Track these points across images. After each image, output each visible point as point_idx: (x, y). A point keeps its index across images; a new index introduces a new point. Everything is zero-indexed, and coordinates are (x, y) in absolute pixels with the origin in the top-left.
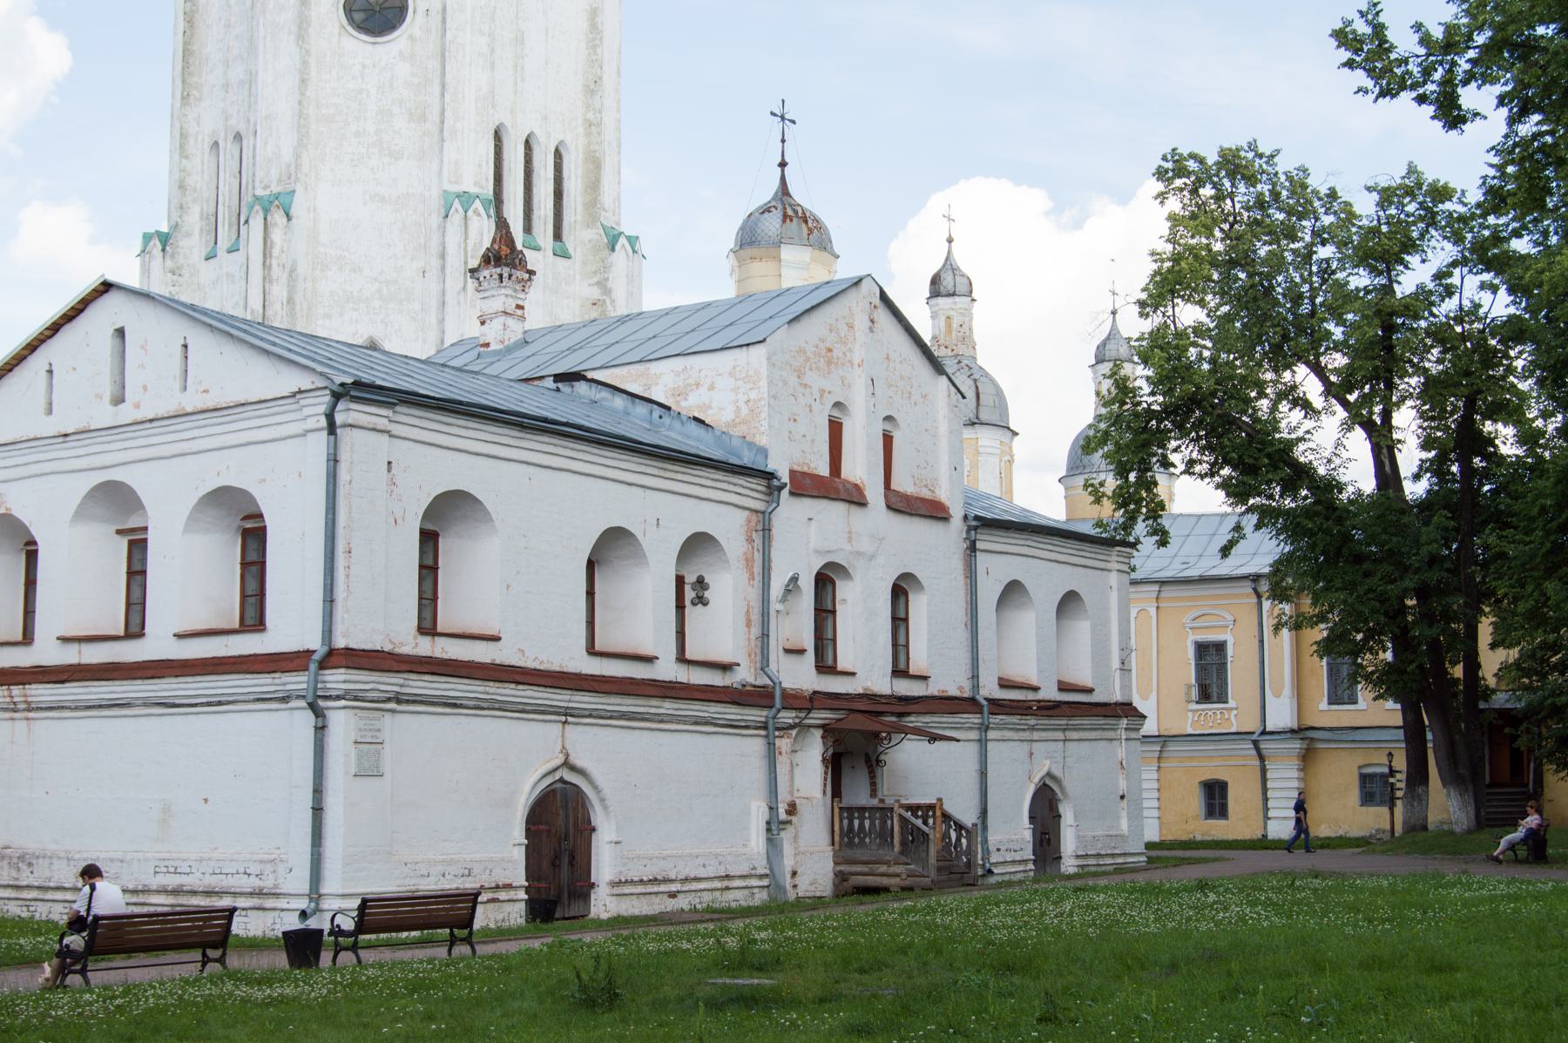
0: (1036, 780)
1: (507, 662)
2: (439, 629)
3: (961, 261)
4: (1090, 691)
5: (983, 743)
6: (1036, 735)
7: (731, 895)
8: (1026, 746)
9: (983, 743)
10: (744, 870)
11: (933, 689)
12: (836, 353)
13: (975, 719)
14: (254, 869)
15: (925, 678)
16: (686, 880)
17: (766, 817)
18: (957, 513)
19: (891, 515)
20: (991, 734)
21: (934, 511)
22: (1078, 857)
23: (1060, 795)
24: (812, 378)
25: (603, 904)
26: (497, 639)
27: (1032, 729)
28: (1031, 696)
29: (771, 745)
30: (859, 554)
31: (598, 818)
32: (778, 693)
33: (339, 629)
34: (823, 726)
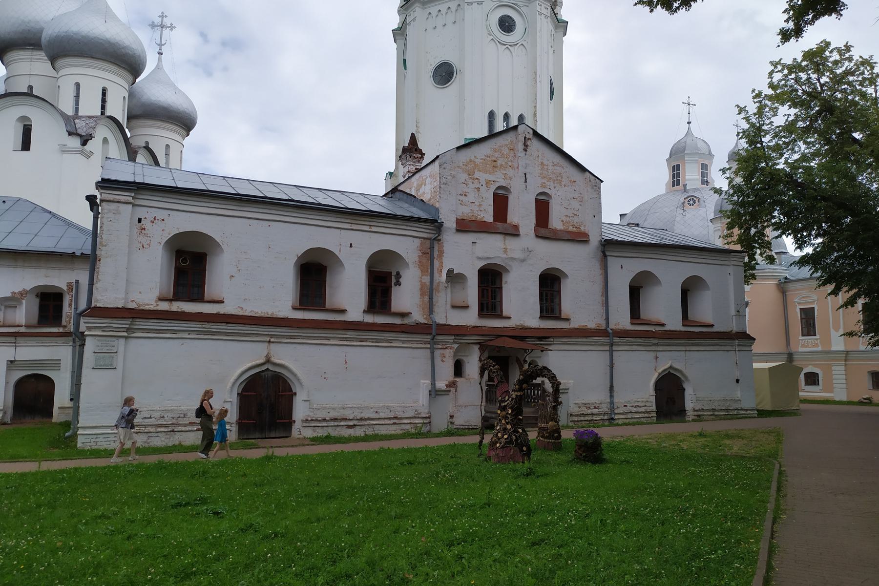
0: (660, 371)
1: (229, 313)
2: (205, 299)
3: (696, 133)
4: (712, 326)
5: (611, 352)
6: (660, 348)
7: (377, 428)
8: (653, 354)
9: (611, 352)
10: (411, 414)
11: (574, 324)
12: (499, 163)
13: (606, 340)
14: (157, 415)
15: (568, 320)
16: (361, 419)
17: (430, 388)
18: (594, 241)
19: (541, 241)
20: (614, 348)
21: (579, 238)
22: (694, 410)
23: (683, 379)
24: (483, 176)
25: (299, 430)
26: (222, 302)
27: (657, 345)
28: (658, 328)
29: (432, 353)
30: (513, 259)
31: (296, 388)
32: (434, 327)
33: (96, 295)
34: (479, 343)
